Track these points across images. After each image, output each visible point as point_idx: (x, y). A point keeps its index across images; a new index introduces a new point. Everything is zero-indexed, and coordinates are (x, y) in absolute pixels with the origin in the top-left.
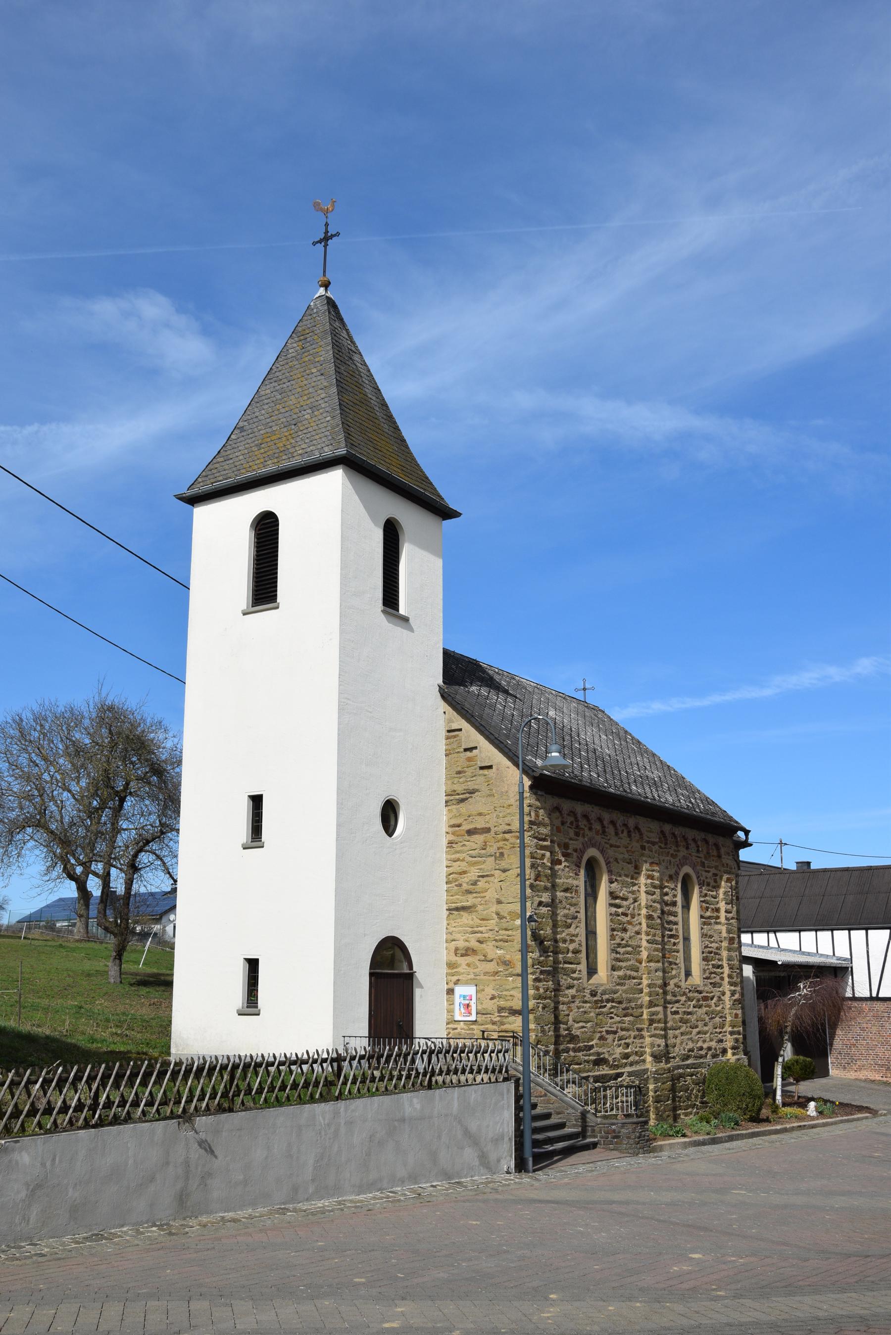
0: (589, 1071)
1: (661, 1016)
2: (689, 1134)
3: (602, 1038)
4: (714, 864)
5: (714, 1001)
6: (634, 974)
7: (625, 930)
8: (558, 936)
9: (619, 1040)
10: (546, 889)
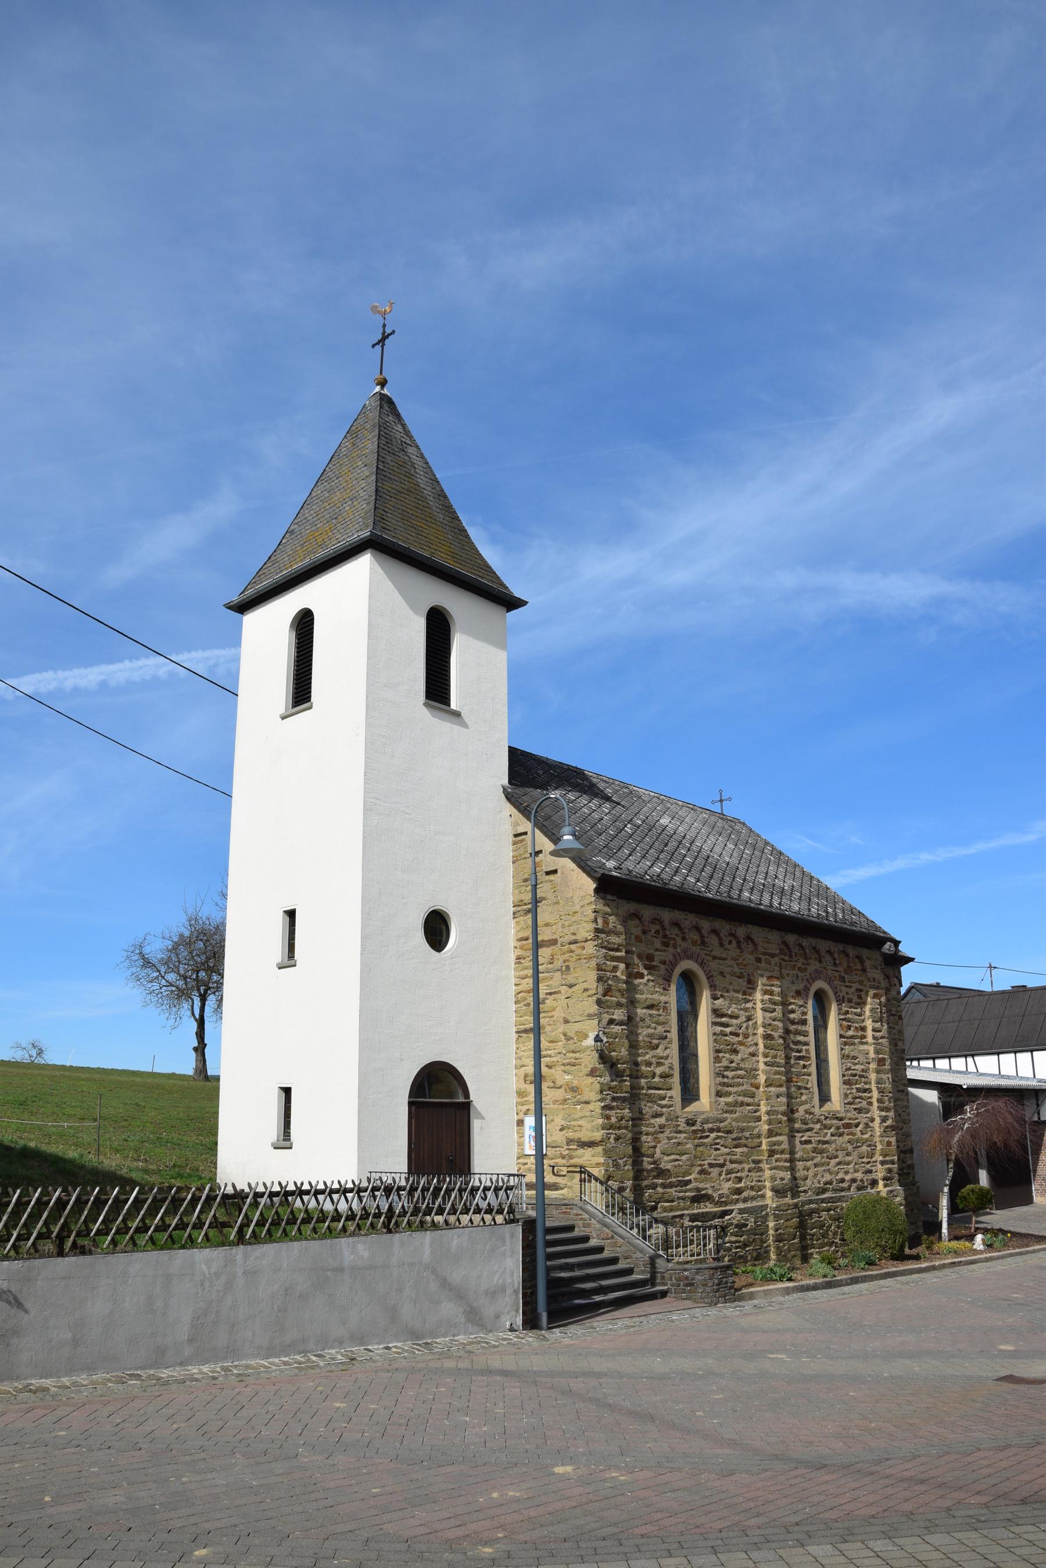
0: (684, 1209)
1: (785, 1146)
2: (799, 1277)
3: (702, 1172)
4: (857, 978)
5: (859, 1128)
6: (750, 1100)
7: (735, 1052)
8: (640, 1059)
9: (726, 1174)
10: (619, 1005)
